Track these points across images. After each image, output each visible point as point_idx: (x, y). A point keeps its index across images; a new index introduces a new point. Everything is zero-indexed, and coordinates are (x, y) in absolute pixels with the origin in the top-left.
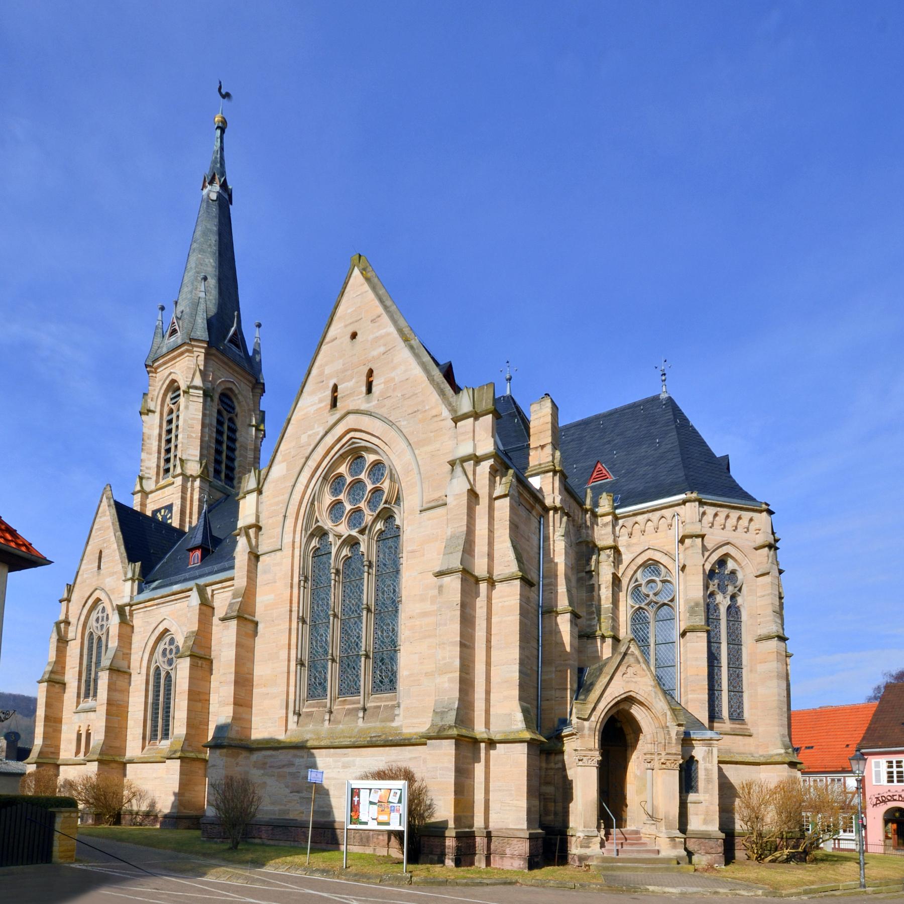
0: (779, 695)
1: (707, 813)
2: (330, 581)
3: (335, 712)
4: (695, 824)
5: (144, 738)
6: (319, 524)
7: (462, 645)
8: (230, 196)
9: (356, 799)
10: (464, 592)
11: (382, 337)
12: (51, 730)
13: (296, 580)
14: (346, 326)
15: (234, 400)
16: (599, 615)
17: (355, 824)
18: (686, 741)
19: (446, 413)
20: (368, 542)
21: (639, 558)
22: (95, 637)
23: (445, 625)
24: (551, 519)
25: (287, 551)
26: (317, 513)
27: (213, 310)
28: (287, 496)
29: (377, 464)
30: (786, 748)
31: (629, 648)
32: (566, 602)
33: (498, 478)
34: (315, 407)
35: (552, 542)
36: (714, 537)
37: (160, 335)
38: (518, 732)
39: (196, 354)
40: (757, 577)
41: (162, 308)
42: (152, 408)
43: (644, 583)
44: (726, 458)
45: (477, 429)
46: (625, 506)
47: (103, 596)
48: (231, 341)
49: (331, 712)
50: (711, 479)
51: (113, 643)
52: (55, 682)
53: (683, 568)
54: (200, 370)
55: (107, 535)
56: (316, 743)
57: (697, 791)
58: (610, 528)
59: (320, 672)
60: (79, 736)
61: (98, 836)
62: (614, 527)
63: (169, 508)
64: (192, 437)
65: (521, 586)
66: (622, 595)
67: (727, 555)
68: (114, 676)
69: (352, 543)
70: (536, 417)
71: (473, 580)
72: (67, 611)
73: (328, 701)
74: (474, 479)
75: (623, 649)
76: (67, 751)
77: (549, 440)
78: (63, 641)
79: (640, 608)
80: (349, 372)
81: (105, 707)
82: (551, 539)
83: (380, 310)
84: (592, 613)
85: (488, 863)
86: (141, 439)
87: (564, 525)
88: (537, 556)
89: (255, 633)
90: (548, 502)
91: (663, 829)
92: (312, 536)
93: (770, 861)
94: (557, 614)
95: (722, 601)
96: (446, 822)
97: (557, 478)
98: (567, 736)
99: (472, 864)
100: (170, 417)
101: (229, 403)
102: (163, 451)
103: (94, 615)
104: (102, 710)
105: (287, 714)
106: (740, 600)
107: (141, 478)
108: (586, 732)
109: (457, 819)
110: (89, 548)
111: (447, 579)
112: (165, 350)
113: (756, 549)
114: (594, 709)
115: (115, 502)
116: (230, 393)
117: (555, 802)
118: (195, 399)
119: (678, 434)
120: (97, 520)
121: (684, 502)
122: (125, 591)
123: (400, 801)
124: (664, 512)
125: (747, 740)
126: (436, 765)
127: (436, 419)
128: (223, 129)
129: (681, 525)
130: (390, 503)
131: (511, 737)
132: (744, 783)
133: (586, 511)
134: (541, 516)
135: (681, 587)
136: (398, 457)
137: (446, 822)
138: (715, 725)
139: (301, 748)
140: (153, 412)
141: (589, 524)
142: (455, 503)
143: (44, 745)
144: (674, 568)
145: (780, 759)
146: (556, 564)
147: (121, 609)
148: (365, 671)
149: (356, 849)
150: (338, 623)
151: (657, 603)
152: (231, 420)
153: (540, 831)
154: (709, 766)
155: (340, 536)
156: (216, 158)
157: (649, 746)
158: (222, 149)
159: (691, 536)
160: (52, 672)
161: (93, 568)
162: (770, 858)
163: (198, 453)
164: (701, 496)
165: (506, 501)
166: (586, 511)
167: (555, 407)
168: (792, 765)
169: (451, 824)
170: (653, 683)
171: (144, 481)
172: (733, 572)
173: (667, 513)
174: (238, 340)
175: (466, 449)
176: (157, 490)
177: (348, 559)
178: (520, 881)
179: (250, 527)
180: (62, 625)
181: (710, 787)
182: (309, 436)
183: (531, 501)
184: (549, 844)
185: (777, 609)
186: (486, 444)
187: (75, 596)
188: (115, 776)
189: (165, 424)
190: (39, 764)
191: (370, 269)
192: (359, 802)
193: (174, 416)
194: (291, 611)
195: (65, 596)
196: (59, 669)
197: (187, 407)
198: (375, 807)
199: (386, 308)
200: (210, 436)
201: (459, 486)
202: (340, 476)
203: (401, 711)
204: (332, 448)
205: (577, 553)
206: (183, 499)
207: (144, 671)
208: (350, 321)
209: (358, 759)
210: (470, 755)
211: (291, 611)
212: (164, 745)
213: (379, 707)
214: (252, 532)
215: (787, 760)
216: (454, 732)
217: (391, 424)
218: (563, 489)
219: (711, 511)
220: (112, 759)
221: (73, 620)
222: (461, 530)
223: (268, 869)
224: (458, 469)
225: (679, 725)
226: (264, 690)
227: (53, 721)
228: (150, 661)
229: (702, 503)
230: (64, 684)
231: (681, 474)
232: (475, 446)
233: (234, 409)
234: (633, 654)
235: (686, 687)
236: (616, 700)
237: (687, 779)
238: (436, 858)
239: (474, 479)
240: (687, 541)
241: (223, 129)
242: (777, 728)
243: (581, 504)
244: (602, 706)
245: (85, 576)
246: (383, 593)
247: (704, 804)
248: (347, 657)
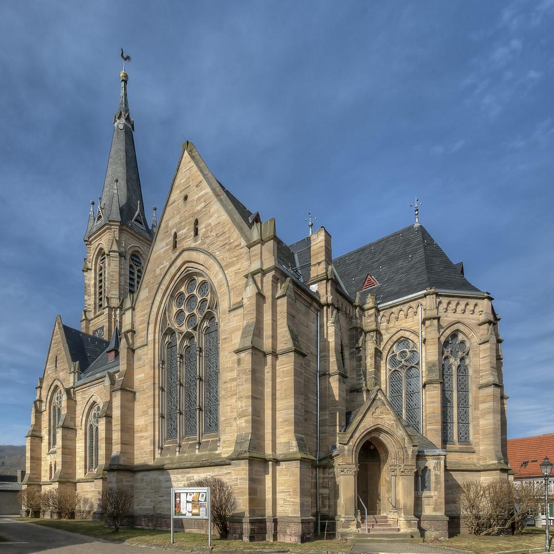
0: (494, 424)
2: (177, 362)
5: (85, 467)
8: (133, 126)
9: (178, 499)
10: (254, 362)
11: (203, 196)
12: (35, 465)
13: (157, 363)
14: (181, 192)
15: (141, 258)
16: (365, 377)
17: (178, 515)
18: (420, 456)
19: (244, 243)
20: (199, 335)
22: (57, 409)
23: (242, 385)
25: (151, 346)
26: (168, 322)
27: (123, 201)
28: (149, 310)
29: (204, 283)
30: (499, 459)
32: (336, 368)
33: (279, 285)
34: (163, 250)
35: (325, 328)
36: (448, 318)
37: (92, 221)
39: (113, 230)
40: (479, 344)
41: (93, 203)
42: (90, 267)
44: (461, 265)
45: (263, 251)
46: (386, 302)
47: (59, 384)
48: (136, 220)
49: (180, 446)
50: (443, 274)
51: (64, 412)
52: (35, 436)
53: (424, 341)
56: (170, 466)
58: (373, 318)
59: (174, 422)
62: (376, 317)
63: (102, 328)
65: (295, 357)
66: (383, 362)
67: (458, 330)
68: (66, 431)
70: (314, 243)
71: (262, 355)
72: (40, 394)
75: (372, 397)
76: (45, 477)
77: (323, 258)
78: (39, 412)
79: (395, 370)
80: (184, 223)
81: (61, 450)
83: (201, 178)
84: (361, 375)
85: (275, 537)
86: (85, 287)
87: (334, 316)
88: (315, 338)
89: (134, 399)
92: (166, 334)
93: (486, 534)
94: (330, 375)
95: (454, 362)
96: (244, 513)
97: (329, 284)
99: (264, 539)
100: (100, 272)
101: (138, 260)
102: (97, 294)
103: (56, 396)
104: (60, 452)
105: (154, 448)
106: (467, 361)
107: (85, 312)
108: (346, 452)
109: (252, 511)
110: (50, 355)
111: (242, 355)
112: (95, 229)
113: (480, 325)
114: (351, 437)
115: (64, 326)
116: (137, 254)
117: (329, 499)
118: (114, 259)
119: (425, 249)
120: (54, 338)
121: (425, 296)
122: (70, 380)
123: (205, 501)
125: (471, 456)
126: (236, 478)
127: (237, 248)
128: (126, 82)
129: (423, 312)
130: (212, 308)
131: (289, 457)
132: (465, 483)
136: (215, 276)
137: (244, 513)
138: (448, 446)
139: (160, 469)
141: (358, 316)
142: (248, 303)
143: (31, 474)
144: (418, 342)
145: (494, 467)
146: (329, 342)
147: (68, 391)
149: (195, 531)
150: (183, 390)
151: (407, 366)
152: (139, 271)
153: (313, 518)
154: (438, 473)
158: (126, 95)
159: (430, 319)
160: (33, 431)
161: (53, 367)
164: (437, 290)
165: (285, 299)
166: (356, 307)
167: (328, 236)
168: (503, 471)
169: (247, 514)
170: (394, 418)
171: (87, 313)
172: (463, 342)
173: (413, 304)
174: (141, 220)
175: (256, 266)
176: (95, 318)
179: (128, 332)
181: (439, 487)
182: (161, 269)
183: (309, 300)
184: (319, 525)
186: (270, 262)
187: (45, 385)
188: (68, 489)
189: (98, 277)
190: (29, 485)
191: (194, 150)
192: (180, 501)
193: (103, 271)
194: (154, 384)
195: (39, 385)
197: (109, 265)
198: (190, 504)
199: (204, 175)
201: (251, 291)
202: (182, 294)
203: (220, 444)
204: (175, 275)
205: (349, 336)
206: (110, 322)
207: (83, 427)
208: (184, 188)
209: (196, 475)
211: (154, 384)
213: (209, 441)
214: (129, 335)
216: (247, 455)
217: (210, 255)
218: (334, 291)
219: (445, 301)
220: (66, 479)
221: (44, 399)
223: (127, 543)
224: (251, 279)
225: (414, 446)
227: (36, 460)
228: (86, 421)
229: (438, 295)
231: (426, 277)
232: (262, 263)
234: (380, 399)
235: (426, 421)
236: (368, 431)
237: (420, 480)
238: (238, 536)
241: (126, 82)
242: (492, 447)
244: (357, 435)
245: (49, 372)
246: (210, 369)
247: (434, 498)
248: (190, 411)
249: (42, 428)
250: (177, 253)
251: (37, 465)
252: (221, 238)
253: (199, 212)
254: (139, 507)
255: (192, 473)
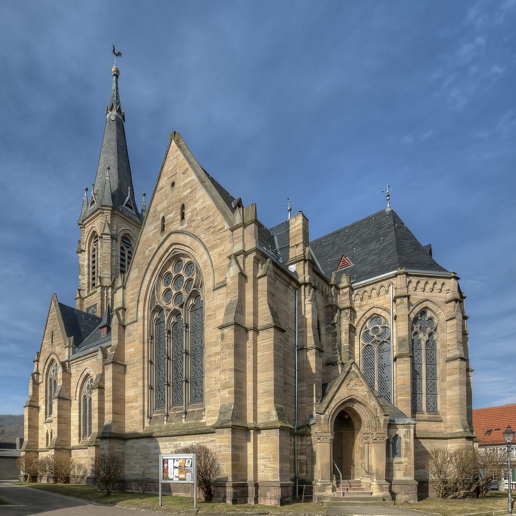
0: (461, 395)
1: (406, 469)
3: (170, 416)
4: (398, 476)
5: (80, 436)
6: (158, 304)
7: (236, 370)
8: (123, 117)
9: (166, 465)
11: (189, 182)
12: (33, 433)
13: (146, 338)
14: (168, 179)
15: (129, 238)
18: (391, 425)
21: (367, 313)
22: (53, 381)
23: (226, 358)
24: (303, 291)
25: (140, 322)
27: (115, 187)
29: (190, 264)
31: (351, 368)
33: (260, 265)
34: (152, 233)
35: (303, 305)
36: (417, 296)
38: (273, 422)
39: (106, 214)
40: (447, 321)
41: (87, 190)
42: (84, 249)
43: (370, 329)
45: (245, 234)
46: (359, 281)
47: (55, 357)
49: (168, 416)
51: (60, 384)
52: (33, 406)
53: (395, 318)
54: (108, 224)
55: (56, 323)
56: (159, 434)
57: (400, 456)
58: (347, 296)
60: (47, 435)
61: (38, 488)
62: (350, 295)
64: (106, 264)
65: (275, 332)
66: (356, 338)
67: (426, 308)
68: (61, 402)
69: (176, 313)
70: (293, 226)
71: (244, 330)
73: (166, 409)
74: (244, 267)
75: (347, 369)
76: (42, 444)
78: (36, 384)
81: (57, 419)
82: (303, 304)
83: (187, 165)
84: (336, 349)
85: (256, 500)
86: (79, 267)
87: (311, 294)
88: (293, 315)
90: (301, 280)
91: (375, 480)
92: (154, 311)
93: (452, 498)
94: (307, 350)
95: (423, 337)
98: (313, 424)
99: (246, 502)
101: (128, 242)
102: (91, 273)
103: (52, 369)
104: (55, 421)
105: (144, 418)
106: (435, 337)
107: (79, 290)
108: (322, 421)
109: (234, 476)
110: (47, 331)
111: (226, 330)
112: (88, 214)
113: (447, 303)
114: (327, 407)
116: (128, 236)
117: (306, 465)
118: (106, 241)
120: (50, 314)
121: (396, 275)
122: (65, 354)
123: (191, 466)
124: (383, 283)
125: (439, 424)
126: (220, 445)
127: (221, 231)
128: (117, 76)
129: (394, 291)
131: (270, 425)
133: (331, 286)
134: (296, 289)
135: (395, 330)
136: (200, 257)
139: (150, 437)
140: (84, 251)
142: (231, 282)
143: (29, 441)
145: (460, 435)
146: (306, 319)
147: (63, 364)
148: (186, 390)
150: (170, 363)
151: (379, 341)
152: (130, 252)
155: (169, 310)
156: (113, 94)
157: (366, 429)
158: (117, 88)
160: (31, 401)
162: (452, 496)
163: (109, 273)
164: (407, 271)
166: (331, 286)
167: (305, 220)
168: (469, 438)
169: (230, 479)
170: (367, 390)
172: (431, 319)
173: (385, 283)
174: (132, 205)
175: (238, 247)
176: (88, 296)
177: (175, 323)
178: (271, 512)
179: (119, 309)
180: (35, 375)
181: (409, 453)
182: (150, 251)
183: (288, 279)
184: (298, 489)
185: (461, 340)
186: (251, 244)
187: (42, 359)
188: (64, 456)
189: (91, 258)
190: (27, 452)
192: (167, 467)
194: (144, 357)
195: (36, 358)
196: (35, 399)
197: (102, 247)
198: (177, 470)
199: (190, 163)
200: (117, 263)
201: (233, 271)
202: (169, 274)
203: (205, 413)
205: (325, 313)
207: (78, 398)
208: (171, 175)
209: (182, 442)
210: (244, 437)
211: (144, 357)
212: (88, 439)
214: (120, 312)
215: (465, 435)
216: (230, 424)
217: (195, 237)
218: (311, 271)
219: (414, 280)
220: (62, 447)
221: (41, 372)
222: (235, 299)
224: (233, 260)
225: (386, 415)
226: (131, 405)
227: (34, 428)
228: (80, 392)
229: (408, 275)
230: (39, 408)
231: (396, 258)
233: (131, 246)
234: (354, 372)
236: (343, 401)
239: (244, 267)
240: (398, 301)
241: (117, 76)
242: (459, 416)
243: (327, 281)
244: (332, 405)
245: (46, 347)
247: (405, 464)
248: (177, 383)
249: (40, 398)
250: (165, 236)
251: (35, 433)
252: (206, 222)
253: (186, 197)
254: (130, 472)
255: (179, 441)
